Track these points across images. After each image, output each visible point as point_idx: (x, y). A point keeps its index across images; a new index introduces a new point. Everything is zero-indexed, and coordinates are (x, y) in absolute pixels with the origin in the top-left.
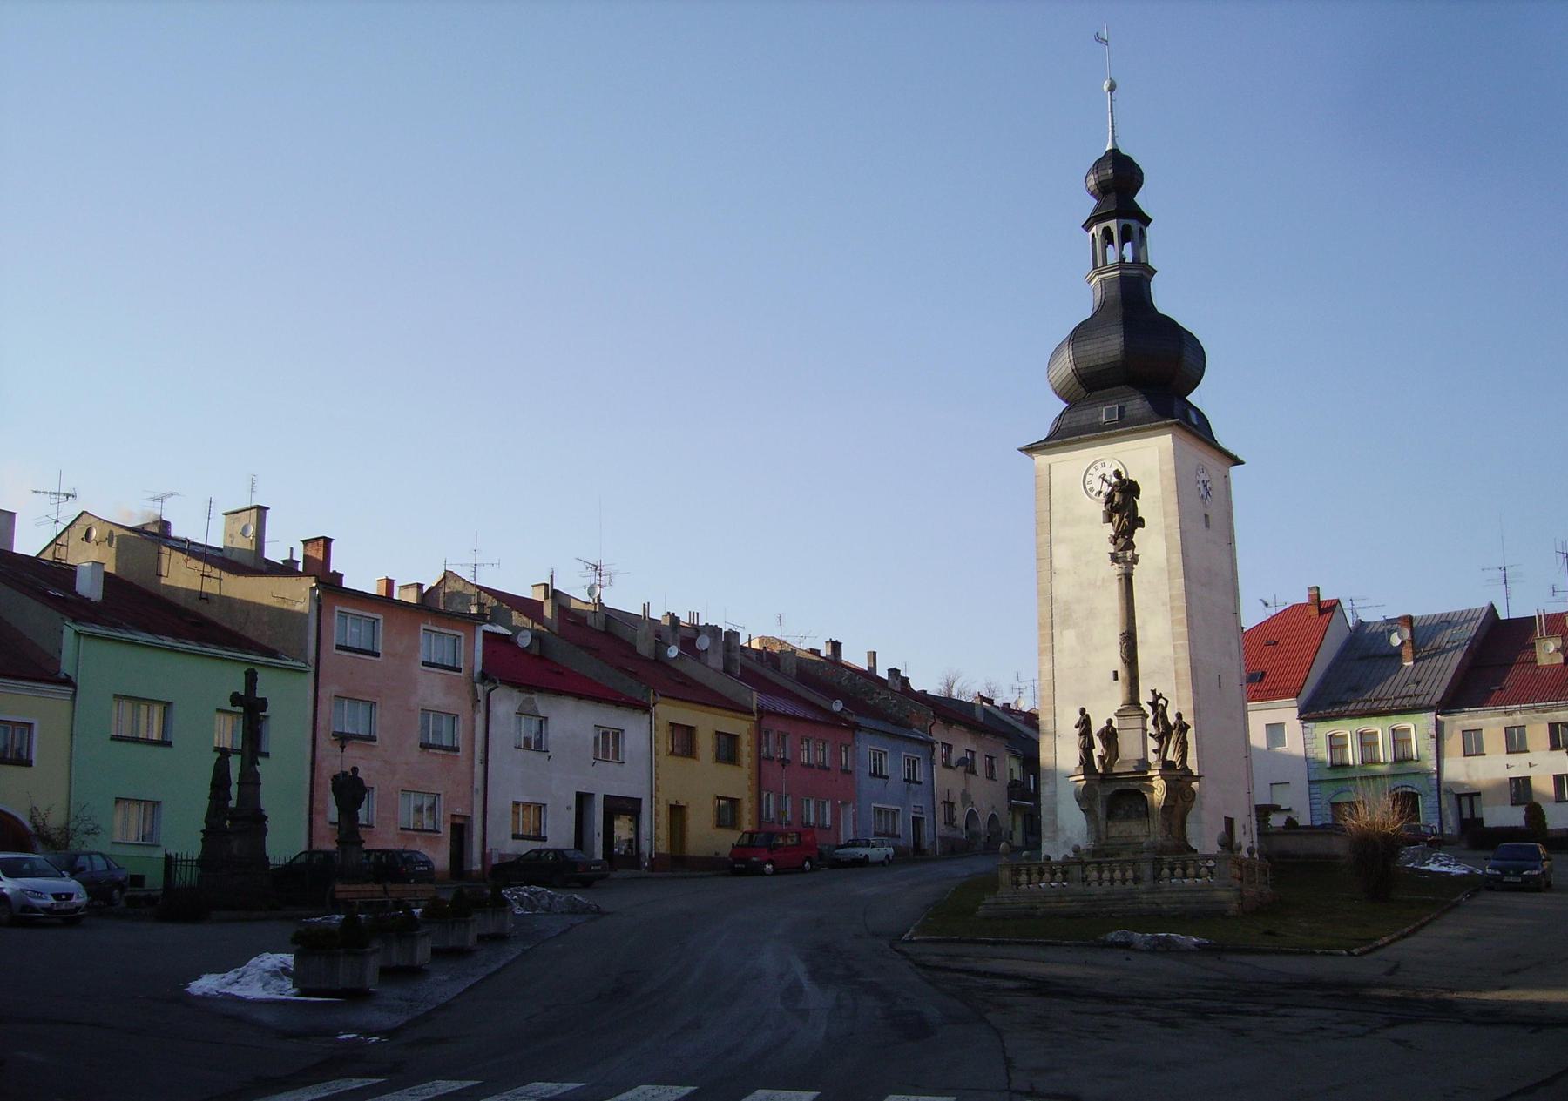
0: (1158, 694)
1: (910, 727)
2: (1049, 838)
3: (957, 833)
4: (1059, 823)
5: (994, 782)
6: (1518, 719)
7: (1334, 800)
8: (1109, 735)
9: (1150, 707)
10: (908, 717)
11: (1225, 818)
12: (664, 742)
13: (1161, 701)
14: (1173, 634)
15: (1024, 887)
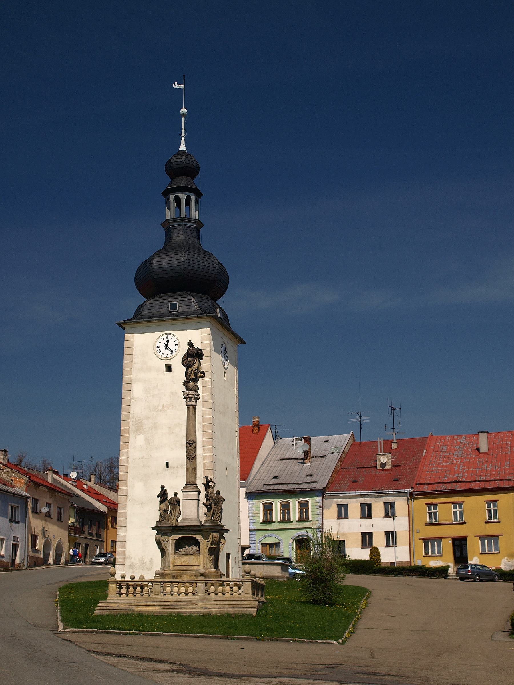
0: (209, 479)
1: (14, 487)
2: (120, 562)
3: (37, 555)
4: (127, 553)
5: (61, 523)
6: (368, 500)
7: (263, 542)
8: (175, 502)
9: (203, 486)
10: (12, 480)
11: (226, 553)
13: (211, 484)
14: (203, 441)
15: (124, 596)
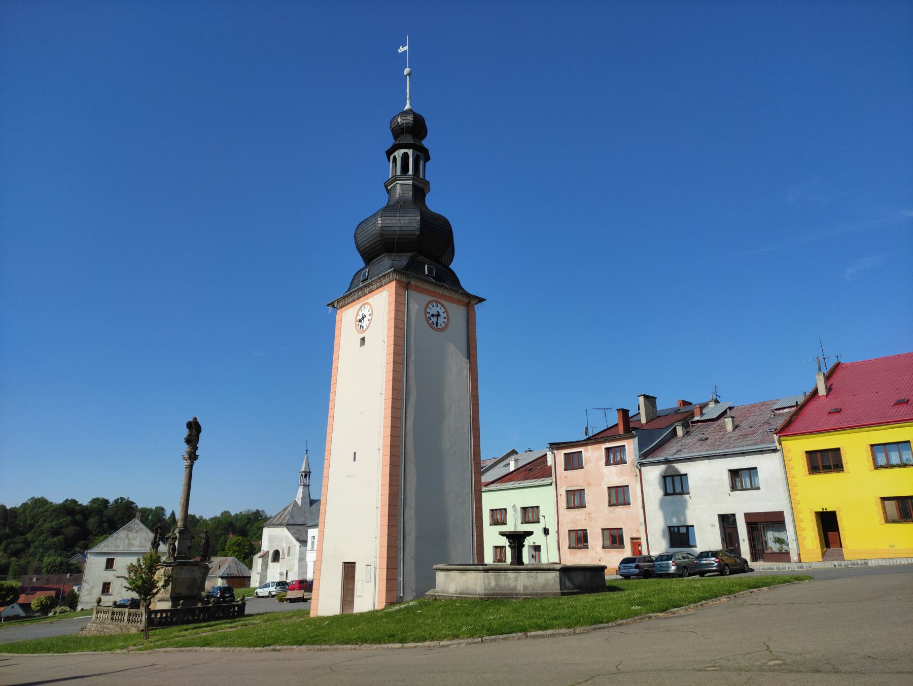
12: (800, 464)
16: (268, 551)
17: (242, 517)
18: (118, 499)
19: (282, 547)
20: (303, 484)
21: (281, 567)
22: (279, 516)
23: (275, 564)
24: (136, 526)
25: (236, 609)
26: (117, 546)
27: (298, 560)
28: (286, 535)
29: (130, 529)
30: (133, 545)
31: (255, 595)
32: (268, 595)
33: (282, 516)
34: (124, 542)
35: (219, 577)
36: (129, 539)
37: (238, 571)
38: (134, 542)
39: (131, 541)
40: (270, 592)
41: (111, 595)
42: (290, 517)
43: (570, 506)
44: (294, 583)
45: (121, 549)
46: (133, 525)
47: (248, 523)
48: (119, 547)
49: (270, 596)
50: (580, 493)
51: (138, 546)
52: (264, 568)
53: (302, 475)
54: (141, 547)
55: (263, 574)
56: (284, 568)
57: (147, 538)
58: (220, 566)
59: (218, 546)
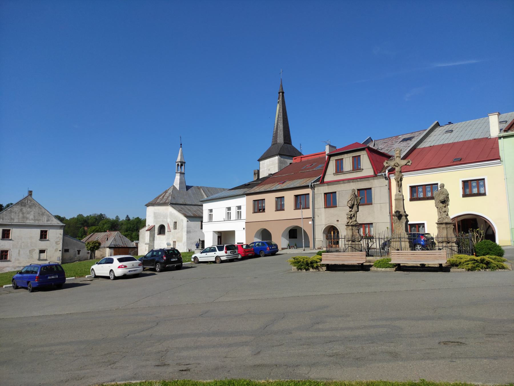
16: (155, 226)
17: (91, 218)
18: (9, 204)
19: (168, 222)
20: (179, 172)
21: (168, 239)
22: (161, 197)
23: (161, 236)
24: (29, 202)
25: (45, 268)
26: (11, 219)
27: (186, 232)
28: (171, 212)
29: (23, 204)
30: (27, 218)
31: (193, 260)
32: (214, 260)
33: (165, 197)
34: (19, 216)
35: (107, 247)
36: (23, 213)
37: (122, 243)
38: (28, 216)
39: (25, 215)
40: (217, 257)
41: (9, 261)
42: (172, 198)
43: (415, 196)
44: (160, 253)
45: (16, 221)
46: (26, 201)
47: (96, 221)
48: (13, 219)
49: (218, 261)
50: (306, 206)
51: (32, 219)
52: (152, 239)
53: (178, 164)
54: (35, 220)
55: (151, 244)
56: (170, 239)
57: (41, 213)
58: (107, 238)
59: (79, 233)
